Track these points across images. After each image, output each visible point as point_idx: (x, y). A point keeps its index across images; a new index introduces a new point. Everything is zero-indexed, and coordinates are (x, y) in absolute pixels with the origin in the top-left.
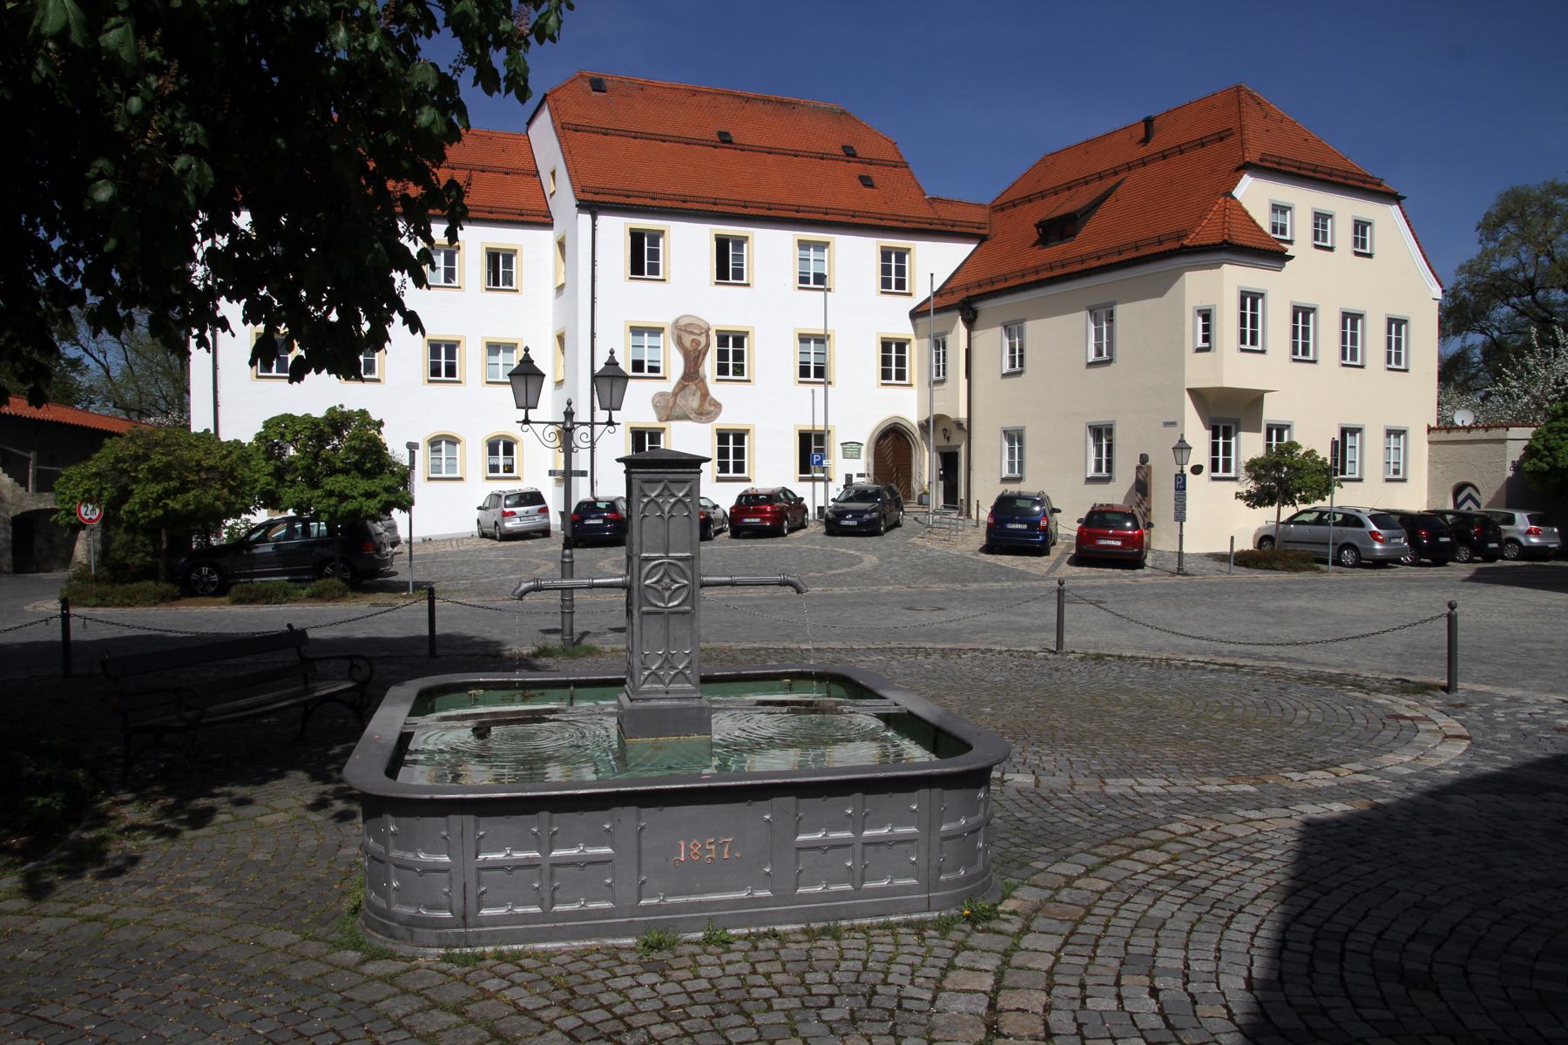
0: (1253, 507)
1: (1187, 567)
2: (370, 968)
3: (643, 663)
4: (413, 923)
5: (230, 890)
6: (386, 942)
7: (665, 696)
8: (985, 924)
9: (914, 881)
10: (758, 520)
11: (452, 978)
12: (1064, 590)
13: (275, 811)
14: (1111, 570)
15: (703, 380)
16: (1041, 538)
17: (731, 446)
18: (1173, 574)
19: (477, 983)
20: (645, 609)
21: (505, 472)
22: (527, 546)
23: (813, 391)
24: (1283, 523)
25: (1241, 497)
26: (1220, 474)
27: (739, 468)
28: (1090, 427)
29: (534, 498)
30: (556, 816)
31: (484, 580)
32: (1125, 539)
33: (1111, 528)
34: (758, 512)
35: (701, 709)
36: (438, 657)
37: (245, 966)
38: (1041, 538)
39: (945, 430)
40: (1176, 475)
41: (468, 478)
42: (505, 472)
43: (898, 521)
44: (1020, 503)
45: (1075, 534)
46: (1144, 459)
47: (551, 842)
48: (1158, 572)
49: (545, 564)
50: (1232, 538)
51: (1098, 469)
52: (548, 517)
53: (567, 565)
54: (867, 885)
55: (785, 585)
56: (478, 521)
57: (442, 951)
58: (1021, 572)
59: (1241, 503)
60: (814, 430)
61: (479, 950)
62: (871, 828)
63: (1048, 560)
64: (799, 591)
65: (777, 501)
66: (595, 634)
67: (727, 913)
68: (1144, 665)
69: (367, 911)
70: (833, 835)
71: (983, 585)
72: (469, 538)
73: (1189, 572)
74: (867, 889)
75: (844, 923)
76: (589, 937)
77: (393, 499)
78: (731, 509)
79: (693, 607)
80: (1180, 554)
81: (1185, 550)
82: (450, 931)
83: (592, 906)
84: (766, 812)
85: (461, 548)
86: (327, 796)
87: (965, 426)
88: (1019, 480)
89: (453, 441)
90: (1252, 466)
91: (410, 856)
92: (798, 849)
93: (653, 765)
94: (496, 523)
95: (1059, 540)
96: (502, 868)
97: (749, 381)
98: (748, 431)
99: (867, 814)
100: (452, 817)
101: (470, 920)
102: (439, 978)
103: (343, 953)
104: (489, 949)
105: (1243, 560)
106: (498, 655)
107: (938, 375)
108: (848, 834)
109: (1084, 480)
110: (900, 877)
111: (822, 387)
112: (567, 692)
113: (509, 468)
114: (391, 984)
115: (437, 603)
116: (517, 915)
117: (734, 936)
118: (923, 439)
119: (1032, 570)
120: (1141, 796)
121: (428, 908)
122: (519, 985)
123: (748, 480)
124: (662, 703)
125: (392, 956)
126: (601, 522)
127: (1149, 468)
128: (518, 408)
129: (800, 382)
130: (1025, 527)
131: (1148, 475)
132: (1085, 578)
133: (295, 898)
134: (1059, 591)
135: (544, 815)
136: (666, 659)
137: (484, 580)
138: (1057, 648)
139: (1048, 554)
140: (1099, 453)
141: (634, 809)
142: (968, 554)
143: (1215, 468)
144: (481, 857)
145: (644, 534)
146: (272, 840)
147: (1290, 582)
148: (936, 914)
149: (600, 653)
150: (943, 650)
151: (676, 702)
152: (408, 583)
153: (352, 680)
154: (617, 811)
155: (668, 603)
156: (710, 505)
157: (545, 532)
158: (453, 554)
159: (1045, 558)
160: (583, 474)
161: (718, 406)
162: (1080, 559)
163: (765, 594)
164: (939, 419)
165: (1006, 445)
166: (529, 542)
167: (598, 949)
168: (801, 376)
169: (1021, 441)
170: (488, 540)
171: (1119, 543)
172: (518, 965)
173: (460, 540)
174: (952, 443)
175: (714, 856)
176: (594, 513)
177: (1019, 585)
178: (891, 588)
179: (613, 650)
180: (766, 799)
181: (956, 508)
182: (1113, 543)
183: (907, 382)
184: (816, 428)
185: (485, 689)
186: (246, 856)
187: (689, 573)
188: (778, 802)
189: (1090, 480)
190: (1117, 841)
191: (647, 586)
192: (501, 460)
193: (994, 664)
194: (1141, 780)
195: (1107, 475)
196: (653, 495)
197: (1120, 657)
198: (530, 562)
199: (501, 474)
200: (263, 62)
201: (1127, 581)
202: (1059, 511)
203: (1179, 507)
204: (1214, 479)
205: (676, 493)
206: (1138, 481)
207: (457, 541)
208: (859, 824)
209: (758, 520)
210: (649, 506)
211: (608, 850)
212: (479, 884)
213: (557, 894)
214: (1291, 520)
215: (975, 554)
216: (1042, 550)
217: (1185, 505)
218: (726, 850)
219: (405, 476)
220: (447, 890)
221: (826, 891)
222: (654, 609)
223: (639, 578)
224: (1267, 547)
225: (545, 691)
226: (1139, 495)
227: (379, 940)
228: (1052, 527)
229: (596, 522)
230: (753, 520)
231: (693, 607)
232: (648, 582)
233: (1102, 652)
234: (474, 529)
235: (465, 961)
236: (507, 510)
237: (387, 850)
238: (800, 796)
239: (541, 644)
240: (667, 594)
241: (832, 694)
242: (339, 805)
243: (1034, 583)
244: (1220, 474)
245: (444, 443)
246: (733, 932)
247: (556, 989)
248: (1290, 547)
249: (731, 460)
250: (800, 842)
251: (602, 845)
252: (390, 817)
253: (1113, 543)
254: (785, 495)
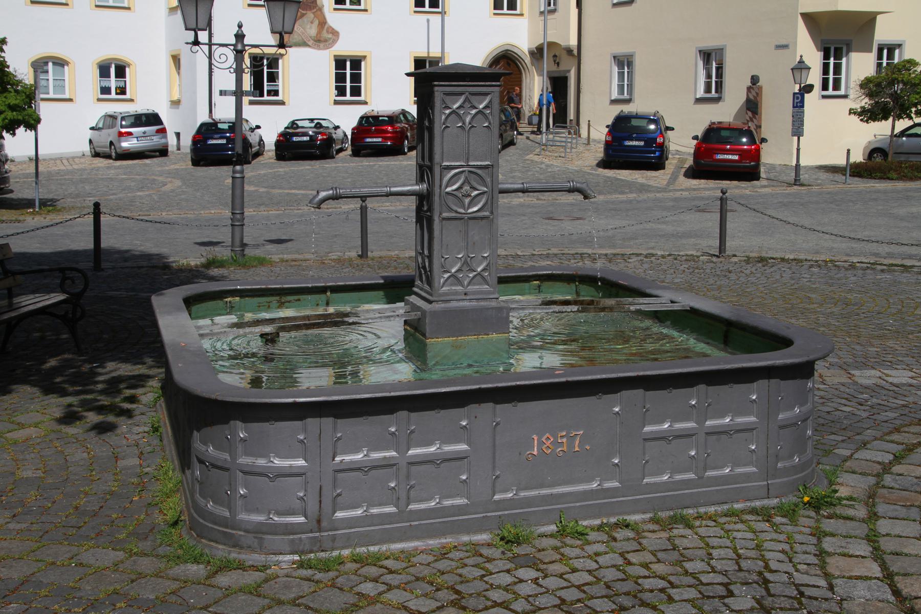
0: (867, 122)
1: (804, 177)
2: (223, 580)
3: (443, 267)
4: (260, 531)
5: (16, 511)
6: (230, 553)
7: (464, 297)
8: (830, 511)
10: (380, 140)
11: (321, 586)
12: (726, 199)
13: (22, 426)
14: (728, 182)
15: (320, 9)
16: (657, 154)
17: (348, 71)
18: (790, 185)
19: (351, 588)
20: (445, 215)
21: (117, 94)
22: (146, 165)
23: (428, 21)
24: (896, 136)
25: (855, 113)
26: (830, 92)
27: (356, 91)
28: (700, 51)
29: (153, 119)
30: (414, 415)
31: (111, 197)
32: (743, 154)
33: (729, 143)
34: (380, 133)
35: (499, 309)
36: (103, 270)
38: (657, 154)
39: (555, 56)
40: (794, 94)
41: (78, 99)
42: (117, 94)
43: (513, 140)
44: (635, 122)
45: (692, 151)
46: (755, 80)
47: (335, 446)
48: (775, 183)
49: (171, 182)
50: (849, 151)
51: (708, 89)
52: (166, 137)
53: (238, 181)
54: (710, 473)
55: (573, 191)
56: (91, 141)
57: (297, 558)
58: (642, 185)
59: (855, 119)
60: (428, 57)
61: (335, 553)
62: (712, 418)
63: (664, 174)
64: (586, 197)
65: (397, 122)
66: (254, 245)
67: (578, 504)
68: (811, 266)
70: (678, 426)
71: (609, 197)
72: (80, 158)
73: (805, 183)
74: (709, 478)
75: (691, 511)
76: (443, 534)
77: (20, 117)
78: (353, 129)
79: (492, 213)
80: (798, 166)
81: (803, 163)
82: (303, 536)
83: (448, 503)
84: (616, 405)
85: (76, 167)
86: (75, 409)
87: (575, 52)
88: (628, 101)
89: (60, 63)
90: (866, 85)
91: (261, 462)
92: (645, 440)
93: (453, 364)
94: (111, 143)
95: (670, 156)
96: (359, 469)
97: (366, 10)
98: (365, 57)
99: (498, 424)
100: (309, 420)
101: (324, 524)
102: (307, 587)
103: (182, 567)
104: (346, 552)
105: (857, 171)
106: (166, 267)
107: (549, 5)
108: (691, 425)
109: (693, 101)
110: (739, 466)
111: (439, 17)
112: (323, 297)
113: (122, 91)
114: (259, 596)
115: (103, 218)
116: (373, 516)
117: (586, 527)
118: (532, 64)
119: (651, 183)
120: (898, 387)
121: (279, 514)
122: (398, 587)
123: (365, 103)
124: (461, 304)
125: (241, 567)
126: (224, 141)
127: (760, 88)
128: (186, 29)
129: (415, 12)
130: (642, 143)
131: (759, 94)
132: (705, 189)
133: (95, 514)
134: (721, 199)
135: (403, 414)
136: (465, 263)
137: (111, 197)
138: (720, 253)
139: (664, 168)
140: (709, 76)
141: (491, 405)
142: (587, 170)
143: (825, 87)
144: (338, 459)
145: (445, 144)
146: (32, 455)
147: (907, 190)
148: (776, 501)
149: (271, 263)
150: (606, 255)
151: (474, 303)
152: (34, 200)
153: (64, 292)
154: (473, 408)
155: (468, 208)
156: (331, 126)
157: (163, 152)
158: (68, 172)
159: (662, 171)
160: (223, 93)
161: (336, 34)
162: (695, 172)
163: (401, 207)
164: (551, 45)
165: (616, 69)
166: (147, 161)
167: (455, 547)
168: (416, 6)
169: (630, 64)
170: (102, 160)
171: (736, 157)
172: (381, 567)
173: (71, 159)
174: (562, 67)
175: (565, 449)
176: (217, 133)
177: (644, 196)
178: (522, 200)
179: (282, 261)
180: (616, 392)
181: (565, 127)
182: (730, 157)
183: (518, 12)
184: (431, 55)
185: (241, 297)
186: (13, 474)
187: (488, 180)
188: (627, 394)
189: (699, 101)
190: (906, 429)
191: (448, 193)
192: (113, 82)
193: (664, 267)
194: (885, 371)
195: (716, 95)
196: (481, 106)
197: (783, 260)
198: (154, 180)
199: (113, 95)
201: (747, 192)
202: (673, 129)
203: (796, 124)
204: (824, 97)
205: (476, 105)
206: (748, 101)
207: (68, 159)
208: (702, 414)
209: (380, 140)
210: (450, 118)
211: (464, 447)
212: (335, 487)
213: (412, 493)
214: (903, 133)
215: (592, 169)
216: (658, 164)
217: (803, 121)
218: (577, 442)
219: (30, 95)
220: (302, 494)
221: (671, 480)
222: (453, 215)
223: (441, 186)
224: (878, 159)
225: (301, 297)
226: (750, 114)
227: (221, 551)
228: (666, 143)
229: (220, 142)
230: (375, 140)
231: (492, 213)
232: (449, 189)
233: (764, 255)
234: (86, 148)
235: (325, 566)
236: (123, 130)
237: (234, 457)
238: (647, 389)
239: (210, 257)
240: (467, 201)
241: (582, 294)
242: (93, 418)
243: (658, 195)
244: (830, 92)
245: (50, 64)
246: (585, 523)
247: (438, 590)
248: (903, 158)
249: (348, 84)
250: (646, 433)
251: (458, 441)
252: (239, 424)
253: (730, 157)
254: (405, 116)
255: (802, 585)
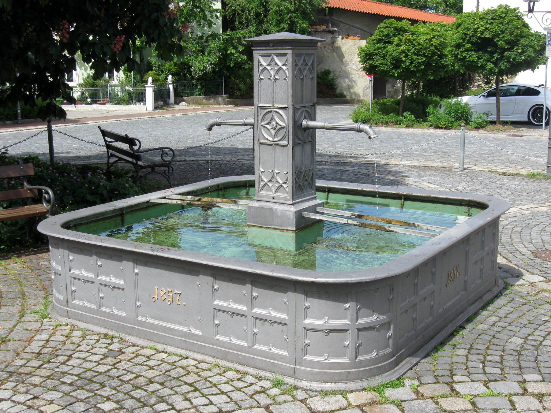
9: (286, 353)
37: (331, 173)
69: (55, 303)
155: (274, 138)
200: (108, 34)
208: (253, 302)
255: (169, 410)
